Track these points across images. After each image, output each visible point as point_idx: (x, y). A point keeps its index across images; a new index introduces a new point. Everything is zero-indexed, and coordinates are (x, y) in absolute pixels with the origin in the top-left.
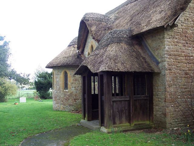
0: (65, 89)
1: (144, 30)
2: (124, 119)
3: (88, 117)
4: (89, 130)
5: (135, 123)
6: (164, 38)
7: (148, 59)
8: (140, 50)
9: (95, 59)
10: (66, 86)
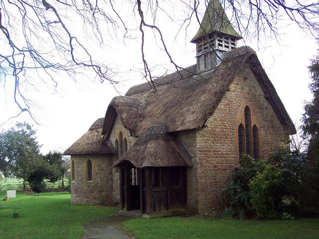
0: (88, 180)
1: (179, 129)
2: (162, 207)
3: (128, 206)
4: (130, 218)
5: (172, 210)
6: (195, 136)
7: (182, 155)
8: (175, 146)
10: (90, 176)
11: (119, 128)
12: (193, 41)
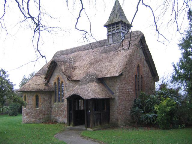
0: (36, 107)
9: (151, 105)
10: (37, 105)
11: (57, 74)
12: (105, 26)
